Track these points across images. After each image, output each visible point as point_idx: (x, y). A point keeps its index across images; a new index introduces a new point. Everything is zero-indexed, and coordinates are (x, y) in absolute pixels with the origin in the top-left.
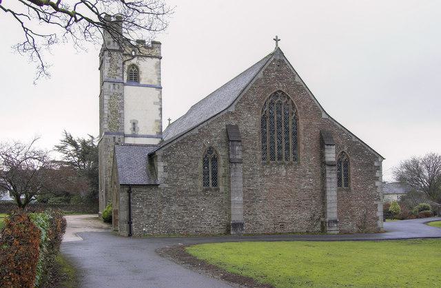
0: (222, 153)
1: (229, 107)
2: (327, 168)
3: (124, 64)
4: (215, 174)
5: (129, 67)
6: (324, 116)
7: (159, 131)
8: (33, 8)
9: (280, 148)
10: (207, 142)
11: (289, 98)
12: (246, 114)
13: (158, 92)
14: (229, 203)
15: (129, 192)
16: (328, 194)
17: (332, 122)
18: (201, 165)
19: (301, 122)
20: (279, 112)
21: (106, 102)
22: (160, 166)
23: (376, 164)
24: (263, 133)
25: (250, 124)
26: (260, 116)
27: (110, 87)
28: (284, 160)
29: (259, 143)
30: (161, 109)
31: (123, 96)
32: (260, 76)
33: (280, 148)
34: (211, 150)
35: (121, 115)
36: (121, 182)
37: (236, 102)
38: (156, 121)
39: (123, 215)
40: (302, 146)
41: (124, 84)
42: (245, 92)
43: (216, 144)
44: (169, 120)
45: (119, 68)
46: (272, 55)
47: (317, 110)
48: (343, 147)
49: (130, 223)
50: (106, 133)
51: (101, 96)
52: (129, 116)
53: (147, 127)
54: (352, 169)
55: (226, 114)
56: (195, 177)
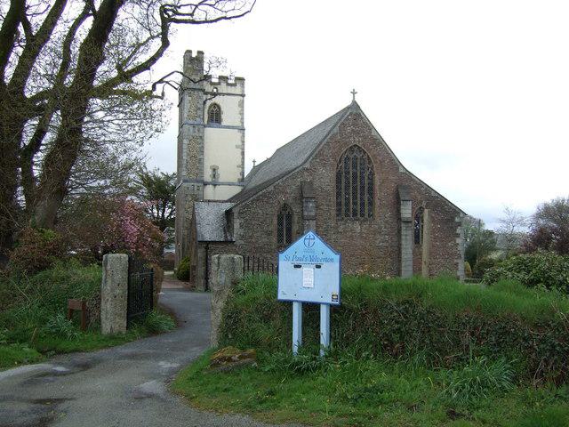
0: (296, 209)
1: (305, 162)
2: (403, 225)
3: (205, 103)
5: (210, 107)
6: (401, 170)
7: (241, 177)
11: (365, 153)
12: (322, 170)
15: (207, 248)
16: (403, 251)
17: (409, 176)
18: (275, 222)
19: (377, 177)
20: (355, 167)
21: (185, 147)
22: (237, 223)
25: (325, 178)
26: (335, 172)
27: (189, 130)
28: (359, 216)
29: (333, 199)
30: (243, 153)
31: (203, 140)
34: (285, 206)
35: (201, 161)
36: (200, 239)
40: (377, 202)
41: (205, 126)
43: (291, 200)
44: (254, 162)
46: (348, 108)
47: (394, 163)
48: (421, 202)
52: (209, 162)
53: (229, 173)
55: (302, 170)
56: (269, 234)
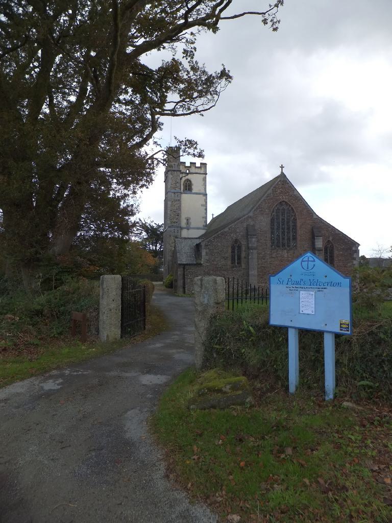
0: (244, 243)
4: (239, 258)
5: (185, 181)
8: (229, 306)
9: (283, 239)
10: (234, 236)
11: (290, 205)
13: (204, 198)
14: (248, 275)
15: (184, 268)
22: (204, 252)
23: (354, 249)
24: (272, 229)
25: (263, 223)
26: (270, 219)
29: (269, 235)
32: (270, 191)
33: (283, 239)
34: (236, 241)
36: (179, 262)
37: (253, 210)
38: (203, 217)
39: (180, 283)
42: (260, 203)
44: (213, 215)
45: (178, 183)
48: (329, 237)
49: (184, 288)
50: (169, 227)
51: (166, 201)
54: (336, 252)
